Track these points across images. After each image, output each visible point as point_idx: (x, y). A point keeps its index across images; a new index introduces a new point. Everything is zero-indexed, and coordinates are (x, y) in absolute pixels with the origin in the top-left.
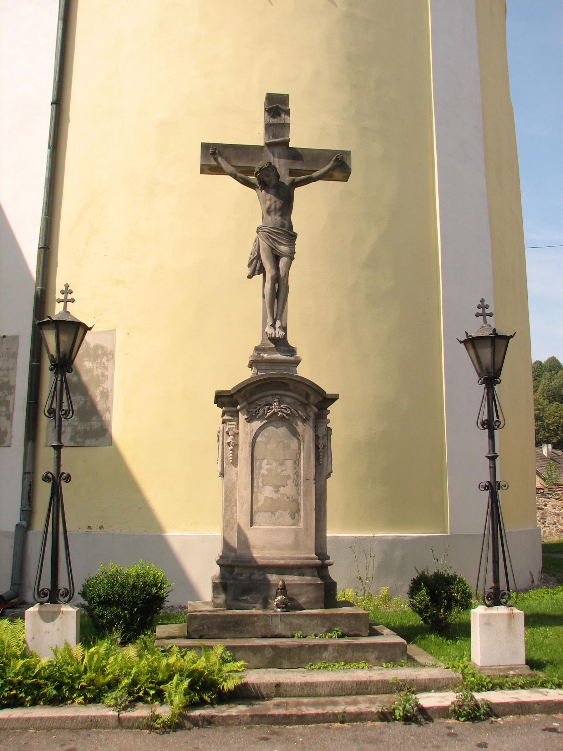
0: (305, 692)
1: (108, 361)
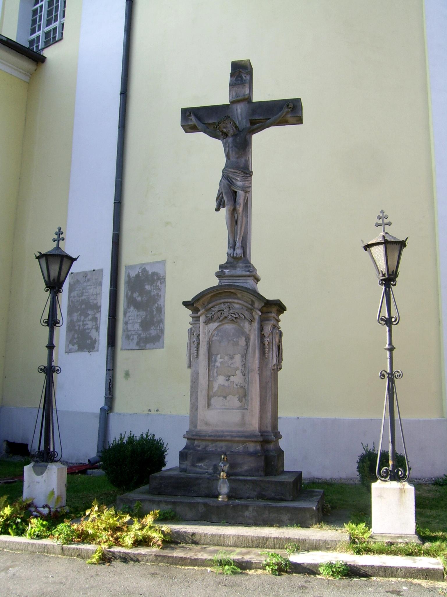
0: (215, 542)
1: (161, 283)
